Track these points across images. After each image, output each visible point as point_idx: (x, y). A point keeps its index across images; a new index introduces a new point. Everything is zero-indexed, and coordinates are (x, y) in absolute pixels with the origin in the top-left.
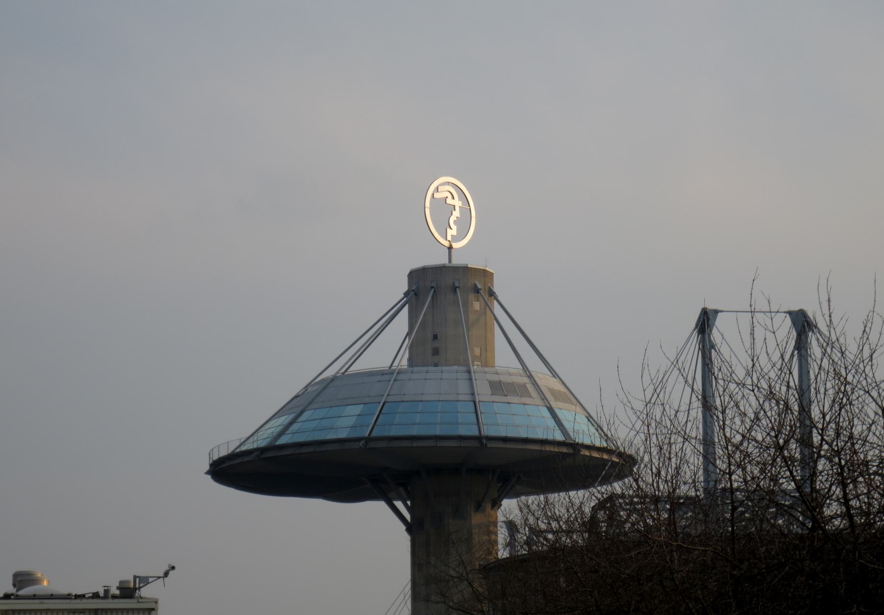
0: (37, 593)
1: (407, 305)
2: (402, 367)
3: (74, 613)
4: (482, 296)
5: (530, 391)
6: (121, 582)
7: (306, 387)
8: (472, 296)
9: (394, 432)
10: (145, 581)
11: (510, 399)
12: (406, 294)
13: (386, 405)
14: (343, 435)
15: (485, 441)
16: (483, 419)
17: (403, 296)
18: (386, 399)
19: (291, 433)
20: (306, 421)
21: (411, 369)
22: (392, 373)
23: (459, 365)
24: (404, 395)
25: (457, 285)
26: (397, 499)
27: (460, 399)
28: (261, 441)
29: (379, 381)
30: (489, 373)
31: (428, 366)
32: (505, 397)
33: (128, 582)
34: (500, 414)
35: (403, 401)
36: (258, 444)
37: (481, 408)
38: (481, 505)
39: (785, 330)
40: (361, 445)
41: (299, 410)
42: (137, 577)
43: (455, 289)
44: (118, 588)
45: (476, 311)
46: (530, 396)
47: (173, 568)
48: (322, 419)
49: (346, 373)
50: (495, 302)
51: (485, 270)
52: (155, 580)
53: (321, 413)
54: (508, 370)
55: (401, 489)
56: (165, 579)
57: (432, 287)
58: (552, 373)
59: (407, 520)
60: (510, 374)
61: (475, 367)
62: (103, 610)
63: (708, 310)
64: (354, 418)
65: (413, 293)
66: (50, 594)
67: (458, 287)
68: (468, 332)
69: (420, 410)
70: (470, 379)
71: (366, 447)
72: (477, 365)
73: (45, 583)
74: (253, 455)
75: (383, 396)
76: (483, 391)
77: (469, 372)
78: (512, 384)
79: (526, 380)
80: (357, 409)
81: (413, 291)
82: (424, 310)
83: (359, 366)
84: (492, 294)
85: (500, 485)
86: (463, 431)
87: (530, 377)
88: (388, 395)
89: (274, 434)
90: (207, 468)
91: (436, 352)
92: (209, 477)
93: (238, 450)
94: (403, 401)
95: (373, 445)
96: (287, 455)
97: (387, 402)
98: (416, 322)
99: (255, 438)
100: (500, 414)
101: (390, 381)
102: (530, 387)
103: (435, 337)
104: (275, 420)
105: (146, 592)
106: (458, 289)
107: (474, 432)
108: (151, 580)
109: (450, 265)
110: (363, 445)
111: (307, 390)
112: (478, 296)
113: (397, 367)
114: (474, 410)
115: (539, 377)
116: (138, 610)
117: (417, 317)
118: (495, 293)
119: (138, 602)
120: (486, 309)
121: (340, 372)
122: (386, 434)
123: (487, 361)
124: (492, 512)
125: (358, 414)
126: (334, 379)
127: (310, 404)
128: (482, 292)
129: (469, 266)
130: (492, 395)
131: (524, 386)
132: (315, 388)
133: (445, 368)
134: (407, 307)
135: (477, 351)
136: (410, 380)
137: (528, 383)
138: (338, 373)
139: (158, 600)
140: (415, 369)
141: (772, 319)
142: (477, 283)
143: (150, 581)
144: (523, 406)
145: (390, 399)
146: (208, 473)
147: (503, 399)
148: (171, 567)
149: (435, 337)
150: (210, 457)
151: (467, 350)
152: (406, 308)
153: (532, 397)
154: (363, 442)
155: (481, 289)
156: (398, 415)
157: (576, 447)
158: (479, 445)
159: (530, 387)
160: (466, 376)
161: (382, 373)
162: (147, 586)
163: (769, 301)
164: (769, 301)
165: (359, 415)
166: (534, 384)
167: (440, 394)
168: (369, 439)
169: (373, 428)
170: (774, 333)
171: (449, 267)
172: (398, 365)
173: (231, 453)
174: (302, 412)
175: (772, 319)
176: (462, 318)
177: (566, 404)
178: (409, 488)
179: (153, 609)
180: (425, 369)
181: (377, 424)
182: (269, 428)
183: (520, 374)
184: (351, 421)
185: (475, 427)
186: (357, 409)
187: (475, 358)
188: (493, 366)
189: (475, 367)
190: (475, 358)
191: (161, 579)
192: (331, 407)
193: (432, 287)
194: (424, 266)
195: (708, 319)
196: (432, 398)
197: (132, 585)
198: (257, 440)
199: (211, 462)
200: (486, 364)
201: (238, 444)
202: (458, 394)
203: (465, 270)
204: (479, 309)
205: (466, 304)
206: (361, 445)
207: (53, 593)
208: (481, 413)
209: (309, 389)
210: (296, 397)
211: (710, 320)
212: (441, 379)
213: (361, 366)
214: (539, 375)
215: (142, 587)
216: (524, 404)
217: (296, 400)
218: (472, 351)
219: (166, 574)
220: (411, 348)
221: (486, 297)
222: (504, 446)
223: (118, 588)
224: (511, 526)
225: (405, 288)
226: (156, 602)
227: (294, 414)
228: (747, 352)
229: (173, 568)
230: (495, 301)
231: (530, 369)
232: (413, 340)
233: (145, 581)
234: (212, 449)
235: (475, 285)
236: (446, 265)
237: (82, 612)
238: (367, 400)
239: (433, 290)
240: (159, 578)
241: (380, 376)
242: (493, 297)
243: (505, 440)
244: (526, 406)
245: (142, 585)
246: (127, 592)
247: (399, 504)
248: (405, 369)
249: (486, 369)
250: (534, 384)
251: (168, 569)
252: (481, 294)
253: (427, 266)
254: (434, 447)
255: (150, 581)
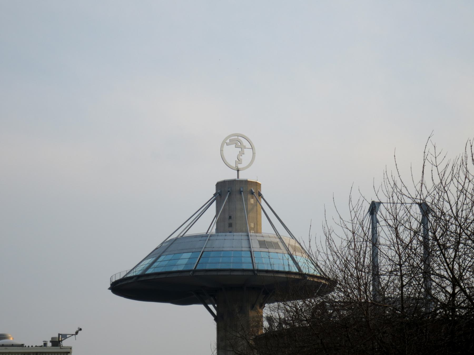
0: (4, 344)
1: (215, 201)
2: (213, 233)
3: (24, 354)
4: (255, 196)
5: (280, 246)
6: (52, 338)
7: (162, 243)
8: (249, 196)
9: (208, 267)
10: (65, 336)
11: (271, 250)
12: (215, 195)
13: (204, 253)
14: (181, 268)
15: (256, 272)
16: (256, 260)
17: (213, 196)
18: (204, 249)
19: (153, 268)
20: (161, 261)
21: (217, 234)
22: (207, 236)
23: (243, 232)
24: (214, 247)
25: (242, 190)
26: (210, 304)
27: (243, 250)
28: (138, 272)
29: (200, 240)
30: (258, 236)
31: (226, 232)
32: (267, 249)
33: (56, 338)
34: (265, 258)
35: (213, 251)
36: (136, 273)
37: (254, 255)
38: (254, 306)
39: (416, 211)
40: (190, 274)
41: (158, 255)
42: (60, 334)
43: (240, 192)
44: (51, 342)
45: (252, 204)
46: (281, 249)
47: (81, 329)
48: (170, 260)
49: (183, 236)
50: (262, 199)
51: (256, 182)
52: (71, 336)
53: (170, 257)
54: (268, 235)
55: (212, 298)
56: (76, 335)
57: (229, 191)
58: (292, 237)
59: (215, 315)
60: (269, 237)
61: (251, 233)
62: (40, 353)
63: (375, 202)
64: (187, 260)
65: (218, 194)
66: (12, 344)
67: (242, 191)
68: (247, 215)
69: (222, 255)
70: (249, 239)
71: (193, 275)
72: (252, 232)
73: (11, 339)
74: (134, 279)
75: (202, 248)
76: (255, 246)
77: (248, 236)
78: (271, 242)
79: (278, 240)
80: (188, 255)
81: (218, 193)
82: (224, 203)
83: (190, 232)
84: (260, 195)
85: (264, 296)
86: (245, 267)
87: (280, 238)
88: (205, 248)
89: (145, 268)
90: (109, 286)
91: (230, 225)
92: (110, 291)
93: (126, 277)
94: (213, 251)
95: (197, 274)
96: (151, 279)
97: (205, 251)
98: (220, 209)
99: (135, 270)
100: (265, 258)
101: (206, 240)
102: (280, 244)
103: (230, 217)
104: (145, 261)
105: (65, 343)
106: (242, 192)
107: (251, 267)
108: (68, 336)
109: (238, 179)
110: (191, 274)
111: (162, 245)
112: (253, 196)
113: (210, 233)
114: (250, 256)
115: (285, 239)
116: (61, 353)
117: (221, 207)
118: (262, 194)
119: (61, 348)
120: (257, 203)
121: (180, 236)
122: (204, 268)
123: (257, 230)
124: (260, 310)
125: (189, 258)
126: (176, 239)
127: (164, 252)
128: (255, 194)
129: (248, 180)
130: (260, 248)
131: (277, 243)
132: (167, 244)
133: (235, 234)
134: (215, 202)
135: (252, 225)
136: (217, 240)
137: (279, 242)
138: (178, 236)
139: (72, 347)
140: (220, 234)
141: (436, 158)
142: (252, 189)
143: (67, 337)
144: (276, 254)
145: (206, 250)
146: (109, 289)
147: (266, 250)
148: (79, 329)
149: (230, 217)
150: (111, 281)
151: (247, 224)
152: (215, 202)
153: (281, 249)
154: (191, 272)
155: (254, 192)
156: (210, 258)
157: (304, 276)
158: (253, 275)
159: (280, 244)
160: (246, 237)
161: (202, 236)
162: (66, 339)
163: (435, 147)
164: (435, 147)
165: (189, 258)
166: (282, 242)
167: (233, 247)
168: (195, 271)
169: (197, 265)
170: (437, 166)
171: (238, 180)
172: (211, 232)
173: (122, 278)
174: (159, 257)
175: (436, 158)
176: (244, 208)
177: (299, 253)
178: (216, 298)
179: (69, 353)
180: (225, 234)
181: (199, 263)
182: (142, 265)
183: (275, 237)
184: (185, 261)
185: (251, 265)
186: (188, 255)
187: (251, 229)
188: (261, 233)
189: (251, 233)
190: (251, 229)
191: (74, 336)
192: (175, 254)
193: (229, 191)
194: (224, 180)
195: (375, 207)
196: (228, 249)
197: (57, 340)
198: (135, 272)
199: (111, 283)
200: (257, 232)
201: (125, 273)
202: (242, 247)
203: (246, 182)
204: (253, 203)
205: (246, 200)
206: (190, 274)
207: (13, 344)
208: (254, 257)
209: (163, 245)
210: (156, 249)
211: (376, 208)
212: (233, 239)
213: (191, 232)
214: (285, 238)
215: (63, 340)
216: (277, 253)
217: (157, 250)
218: (250, 225)
219: (77, 333)
220: (217, 223)
221: (257, 196)
222: (266, 275)
223: (51, 342)
224: (270, 319)
225: (214, 192)
226: (71, 349)
227: (155, 258)
228: (415, 187)
229: (81, 329)
230: (262, 199)
231: (280, 234)
232: (218, 218)
233: (65, 336)
234: (112, 276)
235: (251, 190)
236: (236, 180)
237: (29, 354)
238: (194, 250)
239: (229, 193)
240: (73, 335)
241: (201, 238)
242: (260, 196)
243: (267, 271)
244: (278, 254)
245: (63, 339)
246: (56, 342)
247: (211, 306)
248: (214, 234)
249: (257, 234)
250: (282, 242)
251: (78, 330)
252: (254, 195)
253: (226, 180)
254: (229, 275)
255: (67, 337)
